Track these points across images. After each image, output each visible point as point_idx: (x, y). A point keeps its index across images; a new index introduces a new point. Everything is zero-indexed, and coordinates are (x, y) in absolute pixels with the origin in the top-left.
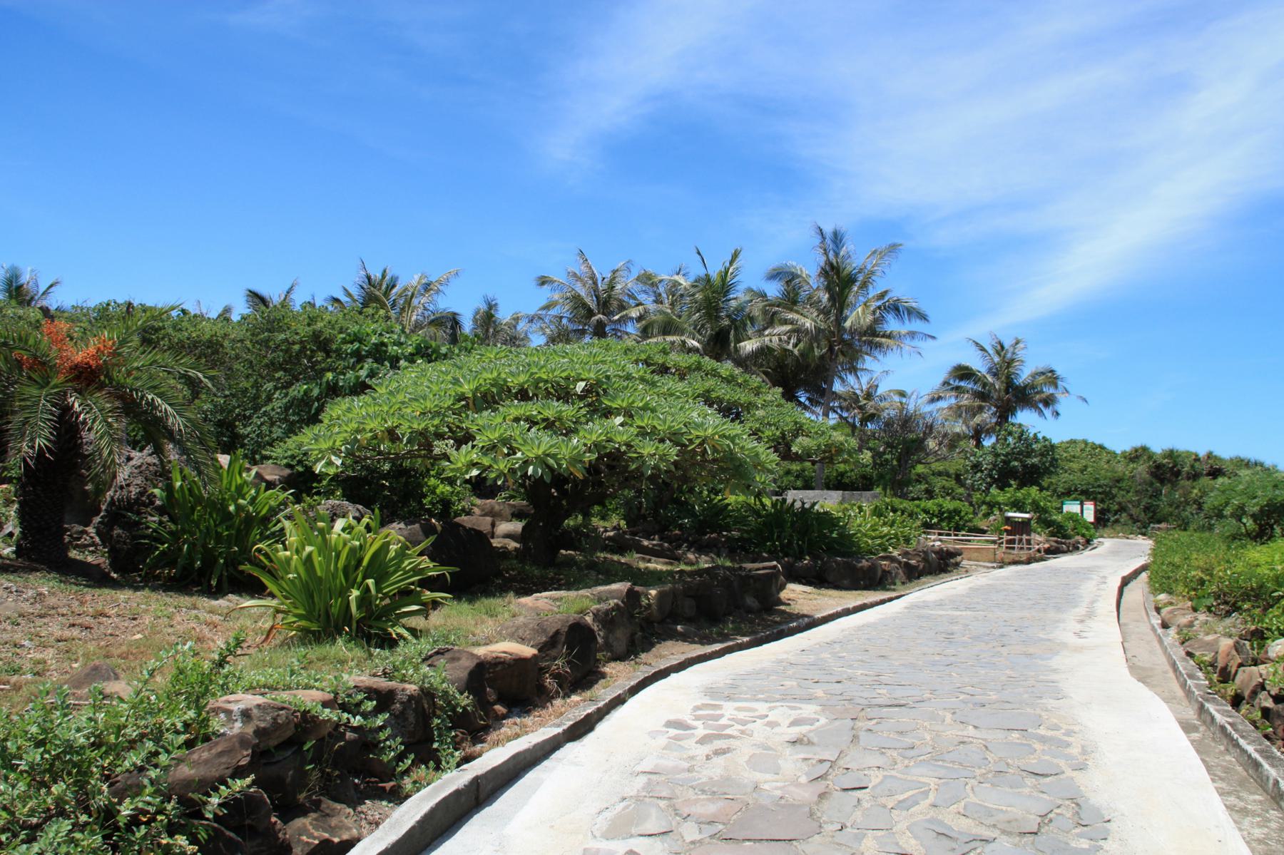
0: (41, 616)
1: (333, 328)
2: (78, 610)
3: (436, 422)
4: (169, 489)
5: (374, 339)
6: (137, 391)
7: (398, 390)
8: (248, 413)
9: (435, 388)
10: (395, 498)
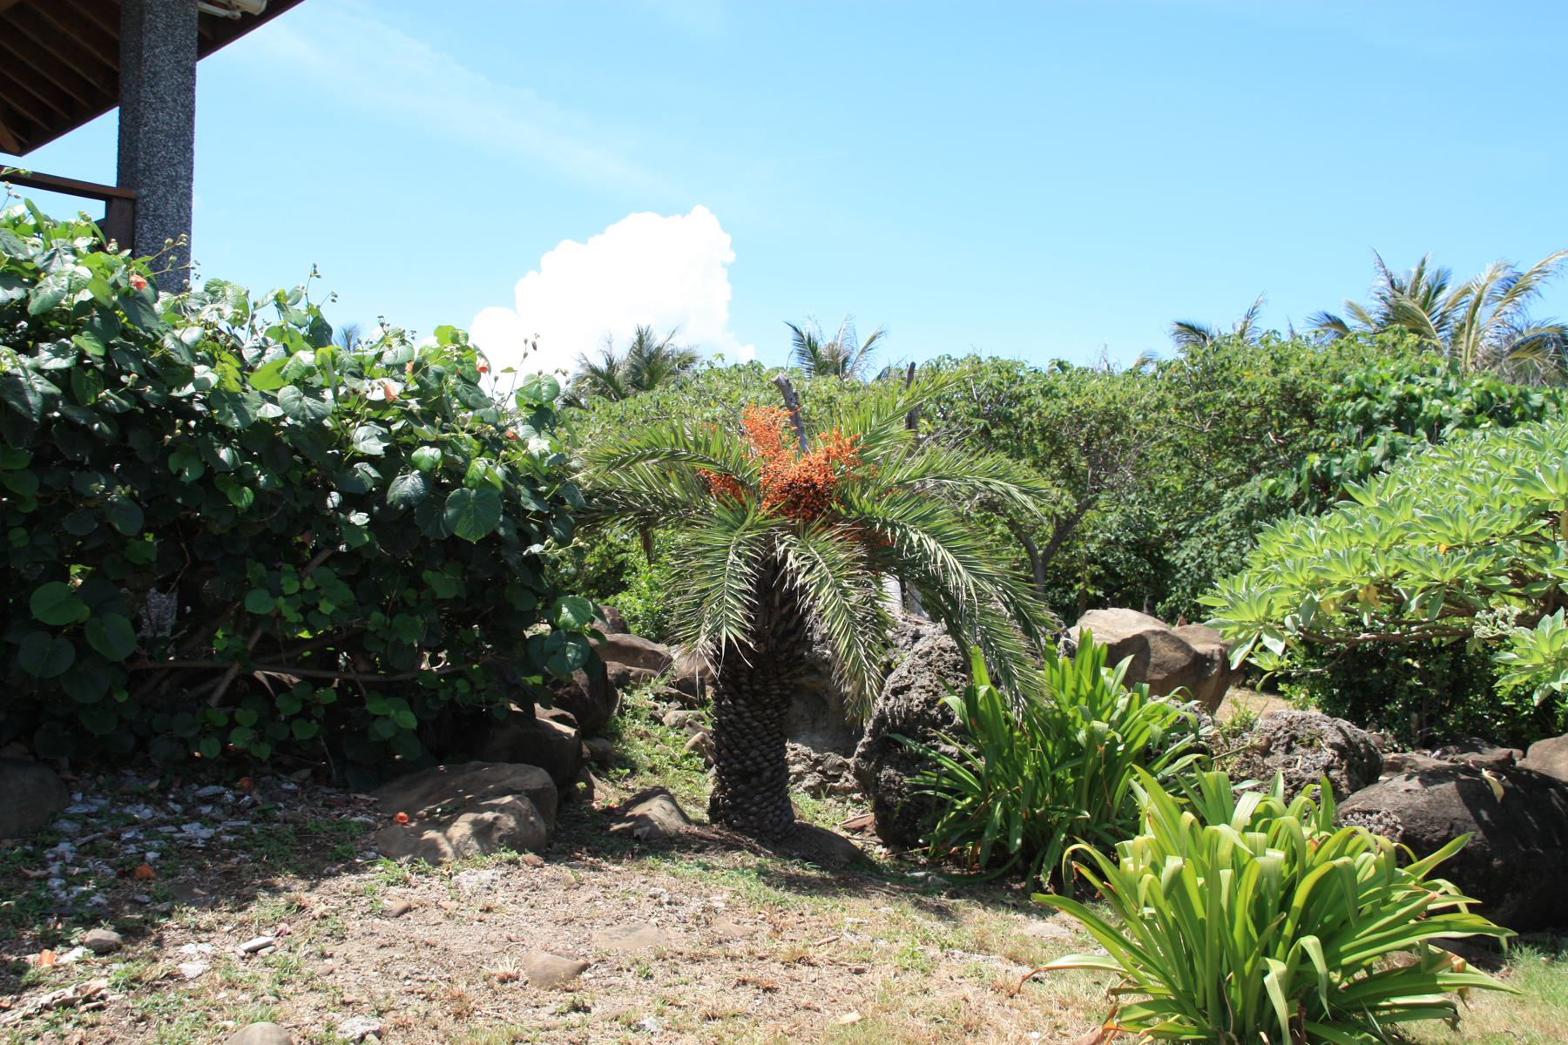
0: (695, 960)
1: (1318, 376)
2: (763, 946)
3: (1482, 565)
4: (969, 696)
5: (1395, 390)
6: (893, 526)
7: (1403, 498)
8: (1180, 527)
9: (1479, 494)
10: (1433, 692)
